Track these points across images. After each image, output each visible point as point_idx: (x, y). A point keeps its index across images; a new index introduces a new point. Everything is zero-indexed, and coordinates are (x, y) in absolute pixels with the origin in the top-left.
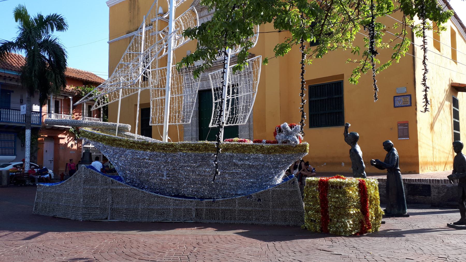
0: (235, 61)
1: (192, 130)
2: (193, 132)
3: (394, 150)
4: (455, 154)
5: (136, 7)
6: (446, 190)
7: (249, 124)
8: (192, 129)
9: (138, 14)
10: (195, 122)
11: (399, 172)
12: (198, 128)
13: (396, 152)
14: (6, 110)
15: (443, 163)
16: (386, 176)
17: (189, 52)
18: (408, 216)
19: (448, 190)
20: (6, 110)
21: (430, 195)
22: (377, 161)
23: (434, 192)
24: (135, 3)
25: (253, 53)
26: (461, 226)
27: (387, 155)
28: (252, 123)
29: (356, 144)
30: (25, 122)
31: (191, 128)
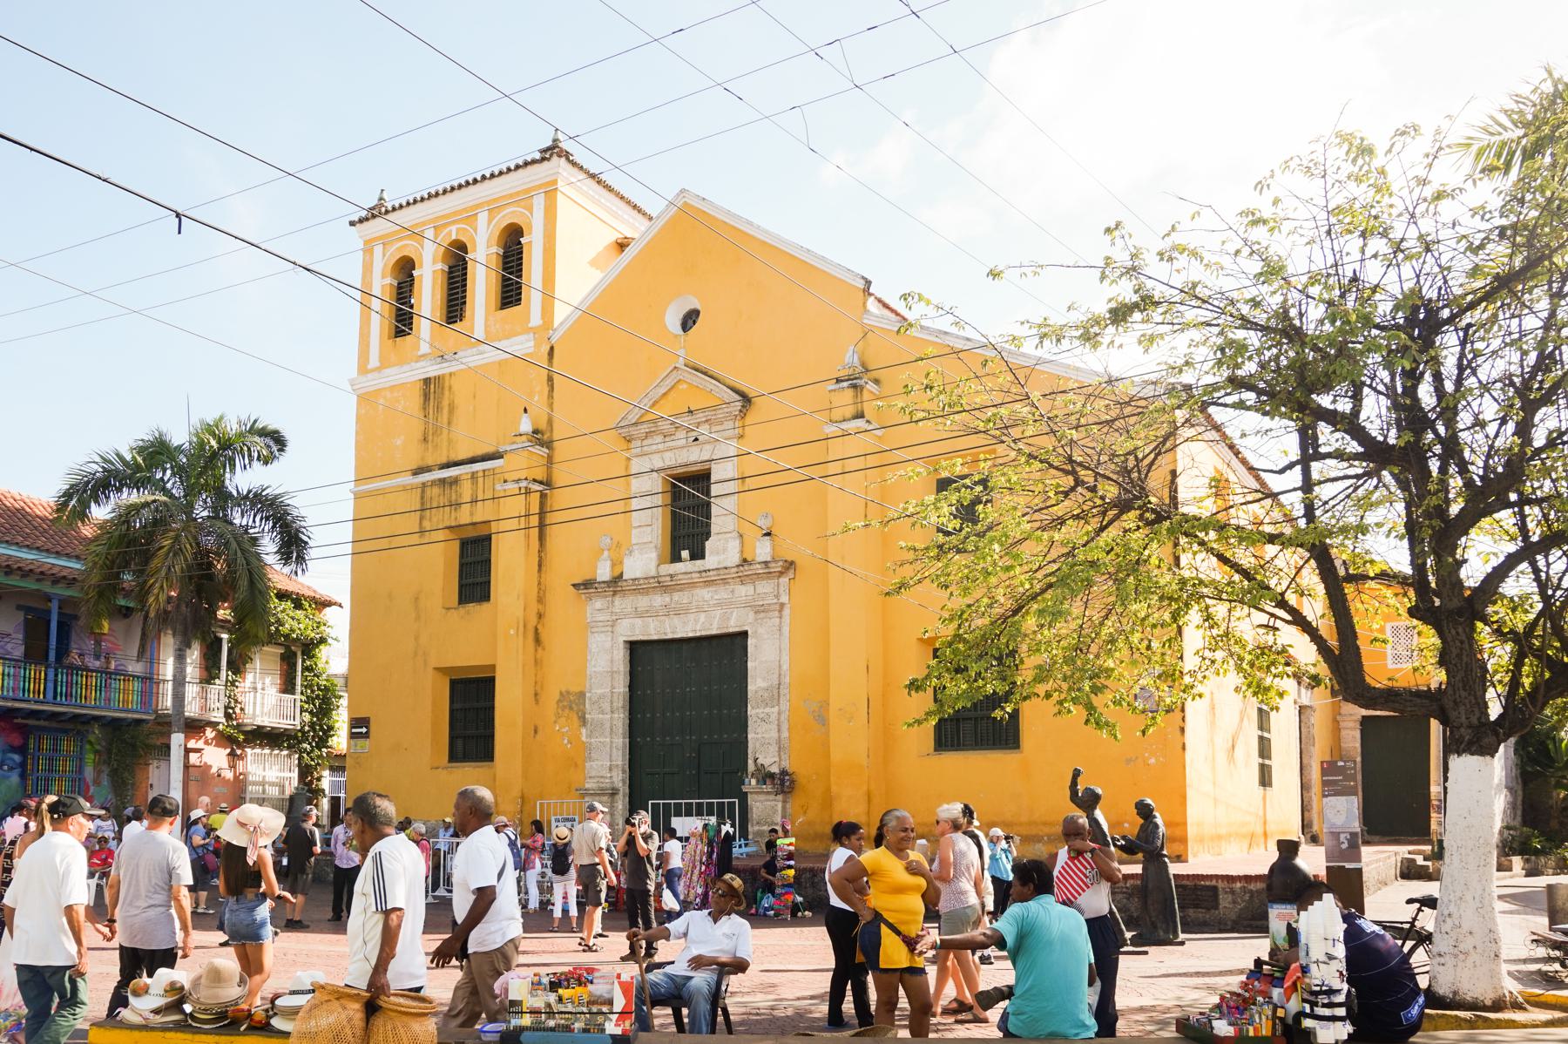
0: (740, 574)
1: (611, 748)
2: (614, 750)
3: (1155, 817)
4: (1346, 926)
5: (445, 403)
6: (1247, 897)
7: (779, 737)
8: (611, 742)
9: (449, 423)
10: (620, 724)
11: (1166, 860)
12: (627, 740)
13: (1159, 820)
14: (33, 667)
15: (549, 475)
16: (1141, 866)
17: (608, 540)
18: (1182, 943)
19: (1251, 897)
20: (33, 667)
21: (1216, 907)
22: (1124, 838)
23: (1225, 901)
24: (443, 394)
25: (789, 559)
26: (1378, 713)
27: (1142, 826)
28: (785, 734)
29: (1095, 808)
30: (44, 697)
31: (608, 740)
